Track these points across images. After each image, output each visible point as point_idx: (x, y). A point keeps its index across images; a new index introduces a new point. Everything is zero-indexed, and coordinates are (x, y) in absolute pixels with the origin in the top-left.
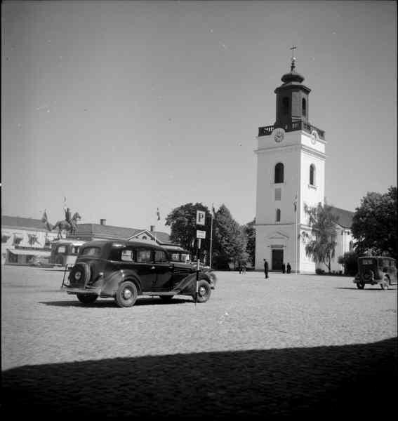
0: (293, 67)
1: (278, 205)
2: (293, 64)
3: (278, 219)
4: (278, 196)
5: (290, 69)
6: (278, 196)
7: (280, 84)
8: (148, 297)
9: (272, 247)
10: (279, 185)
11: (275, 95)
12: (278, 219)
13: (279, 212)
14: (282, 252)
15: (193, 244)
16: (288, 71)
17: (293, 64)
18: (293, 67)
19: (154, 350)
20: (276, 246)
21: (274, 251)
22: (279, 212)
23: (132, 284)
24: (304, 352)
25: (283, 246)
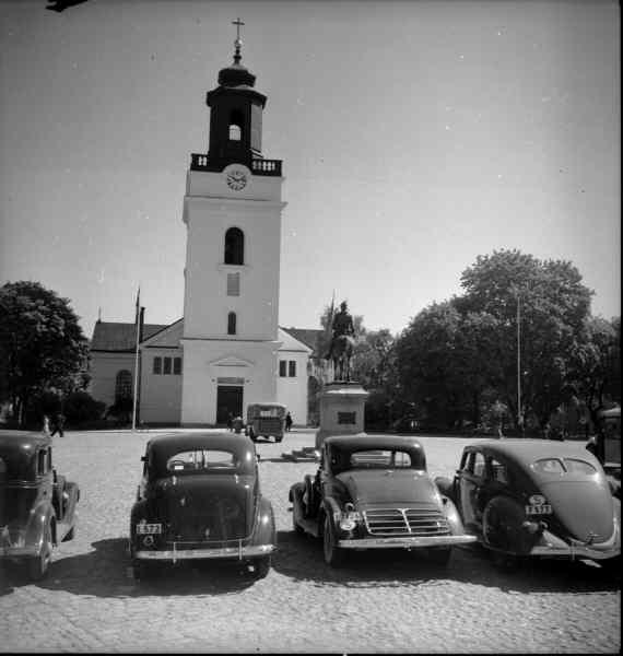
0: (237, 58)
1: (232, 304)
2: (238, 52)
3: (232, 329)
4: (233, 288)
5: (233, 61)
6: (233, 288)
7: (214, 85)
8: (326, 525)
9: (220, 380)
10: (233, 269)
11: (208, 110)
12: (232, 329)
13: (232, 318)
14: (239, 391)
15: (20, 421)
16: (229, 63)
17: (238, 52)
18: (237, 58)
19: (141, 642)
20: (230, 380)
21: (220, 389)
22: (232, 318)
23: (505, 500)
24: (57, 585)
25: (242, 381)
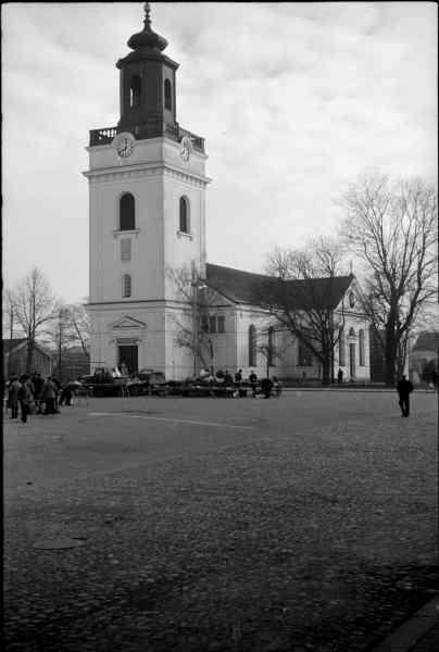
0: (147, 22)
2: (147, 16)
3: (128, 295)
4: (126, 254)
6: (126, 254)
12: (128, 295)
13: (128, 279)
17: (147, 16)
18: (147, 22)
22: (128, 279)
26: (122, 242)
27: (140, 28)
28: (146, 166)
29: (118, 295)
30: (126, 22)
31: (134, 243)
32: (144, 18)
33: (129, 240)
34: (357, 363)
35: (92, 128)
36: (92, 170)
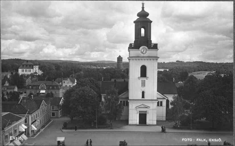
0: (143, 8)
2: (143, 6)
3: (143, 97)
4: (143, 84)
6: (143, 84)
10: (144, 79)
12: (143, 97)
13: (143, 93)
17: (143, 6)
18: (143, 8)
22: (143, 93)
25: (146, 112)
26: (142, 80)
27: (140, 10)
28: (133, 58)
29: (140, 97)
30: (137, 7)
31: (146, 81)
32: (142, 7)
33: (145, 81)
34: (37, 116)
35: (158, 46)
36: (130, 57)
